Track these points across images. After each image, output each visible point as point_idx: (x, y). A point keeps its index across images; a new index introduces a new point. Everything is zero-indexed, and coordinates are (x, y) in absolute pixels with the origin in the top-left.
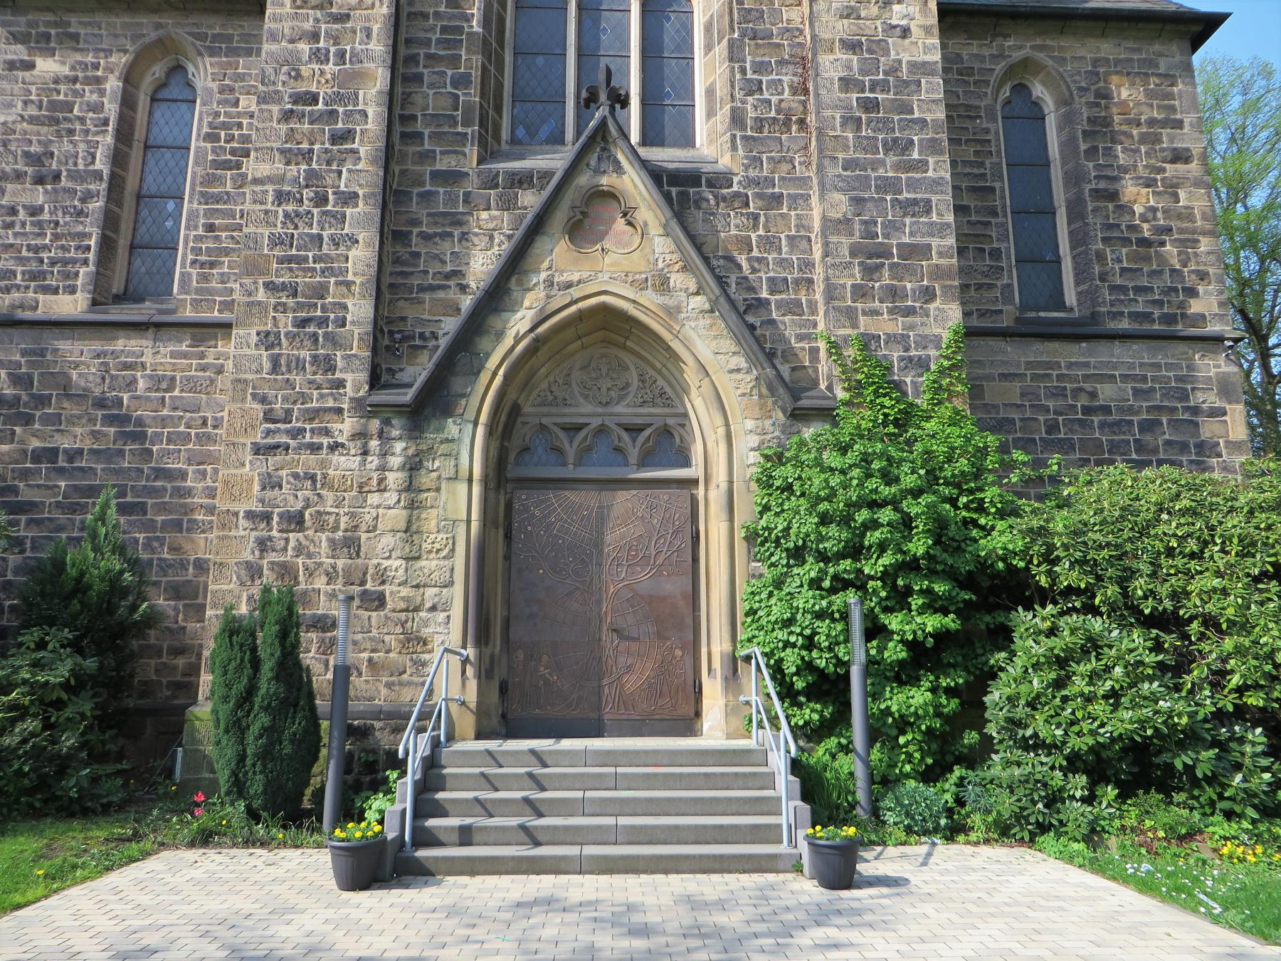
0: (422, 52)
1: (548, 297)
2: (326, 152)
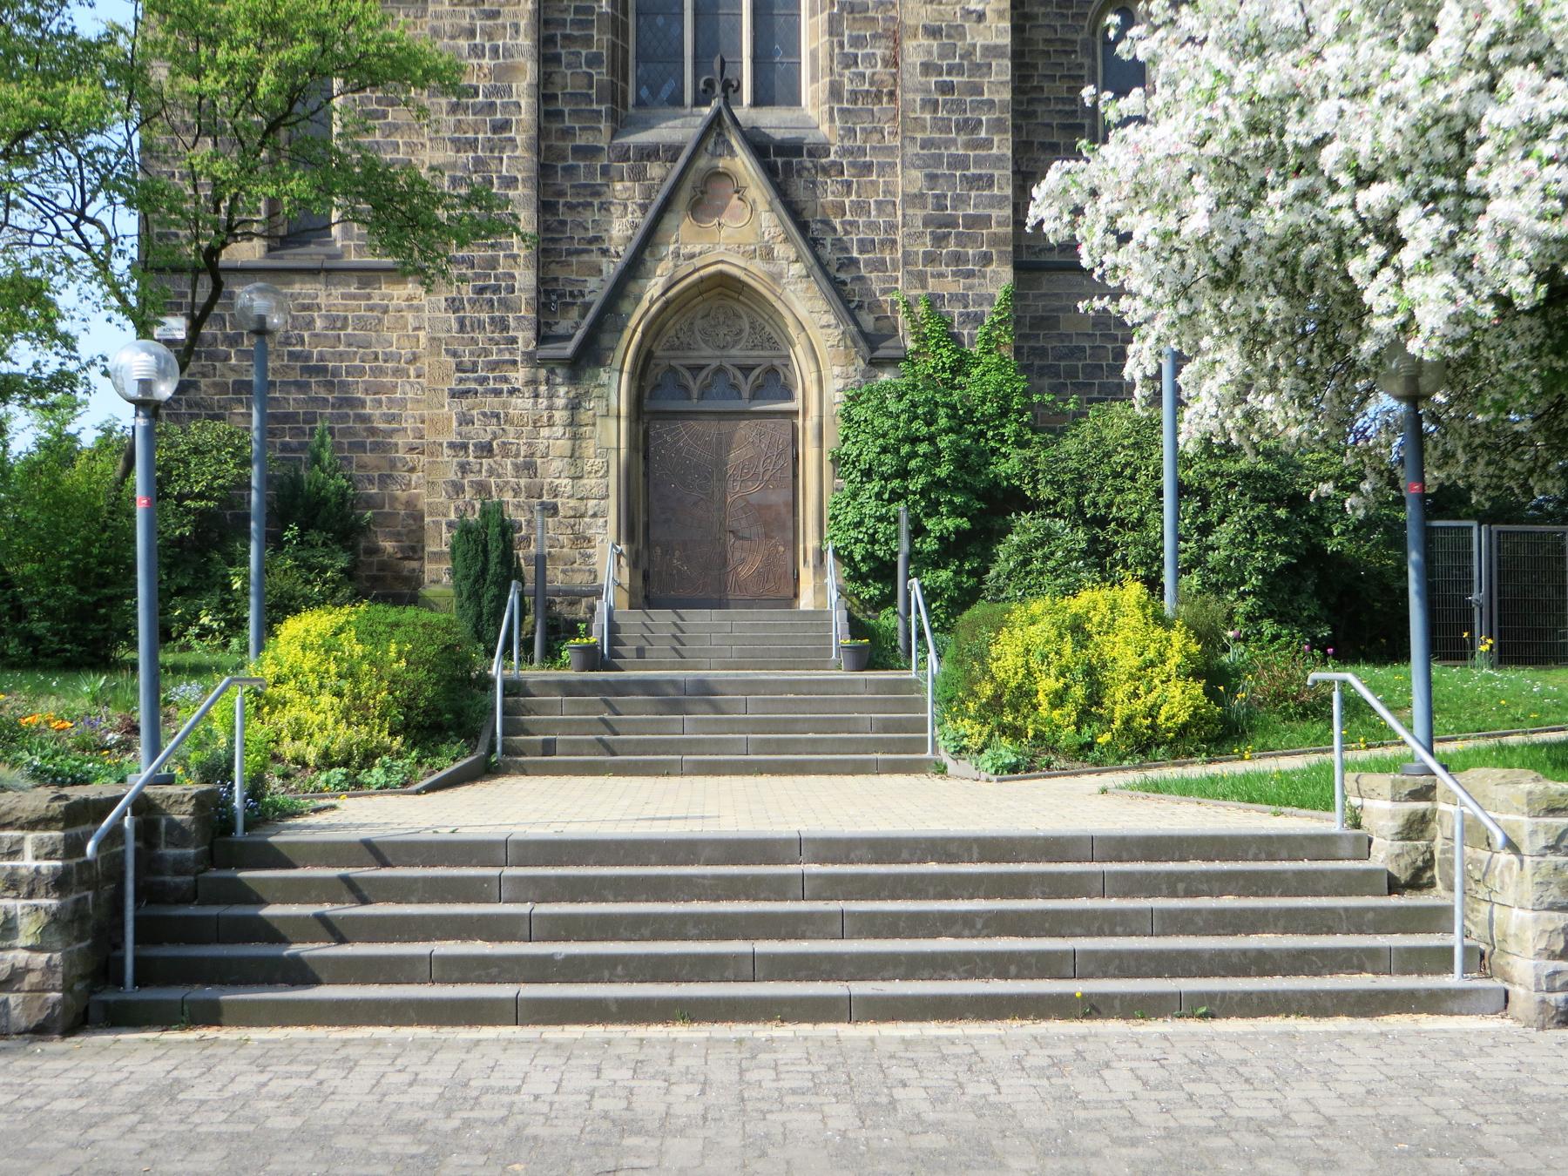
0: (558, 33)
1: (676, 266)
2: (489, 140)
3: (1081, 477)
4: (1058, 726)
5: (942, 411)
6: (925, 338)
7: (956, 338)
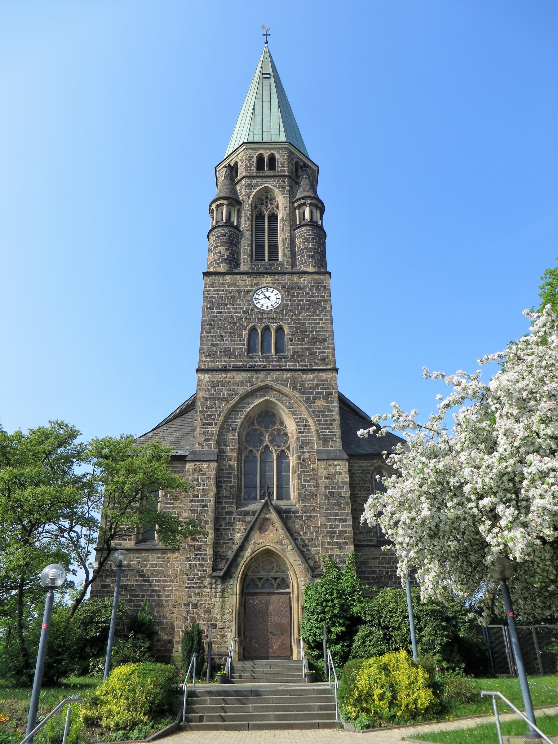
3: (379, 613)
4: (382, 708)
5: (335, 591)
6: (329, 568)
7: (338, 568)
